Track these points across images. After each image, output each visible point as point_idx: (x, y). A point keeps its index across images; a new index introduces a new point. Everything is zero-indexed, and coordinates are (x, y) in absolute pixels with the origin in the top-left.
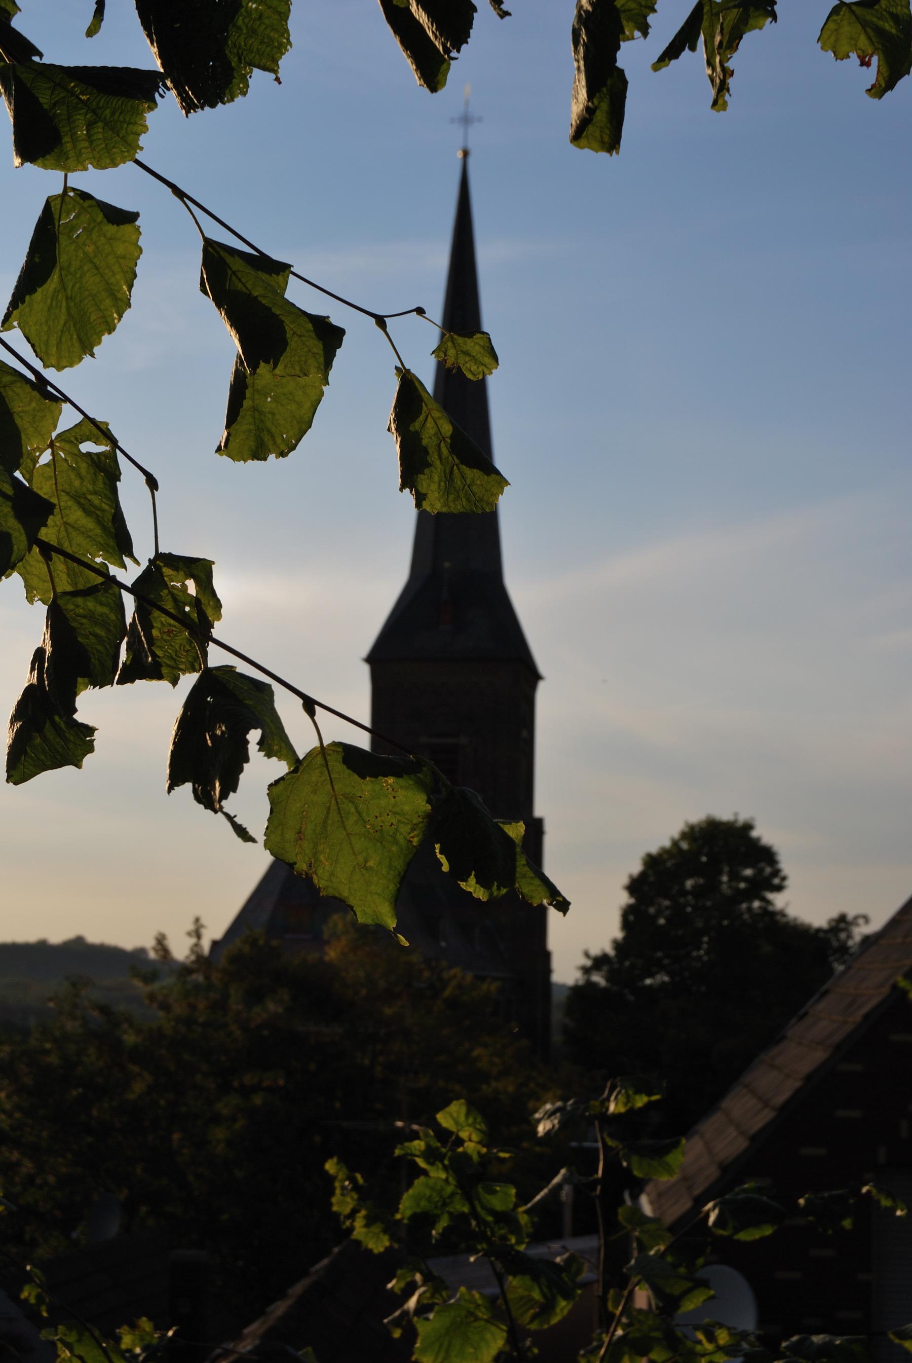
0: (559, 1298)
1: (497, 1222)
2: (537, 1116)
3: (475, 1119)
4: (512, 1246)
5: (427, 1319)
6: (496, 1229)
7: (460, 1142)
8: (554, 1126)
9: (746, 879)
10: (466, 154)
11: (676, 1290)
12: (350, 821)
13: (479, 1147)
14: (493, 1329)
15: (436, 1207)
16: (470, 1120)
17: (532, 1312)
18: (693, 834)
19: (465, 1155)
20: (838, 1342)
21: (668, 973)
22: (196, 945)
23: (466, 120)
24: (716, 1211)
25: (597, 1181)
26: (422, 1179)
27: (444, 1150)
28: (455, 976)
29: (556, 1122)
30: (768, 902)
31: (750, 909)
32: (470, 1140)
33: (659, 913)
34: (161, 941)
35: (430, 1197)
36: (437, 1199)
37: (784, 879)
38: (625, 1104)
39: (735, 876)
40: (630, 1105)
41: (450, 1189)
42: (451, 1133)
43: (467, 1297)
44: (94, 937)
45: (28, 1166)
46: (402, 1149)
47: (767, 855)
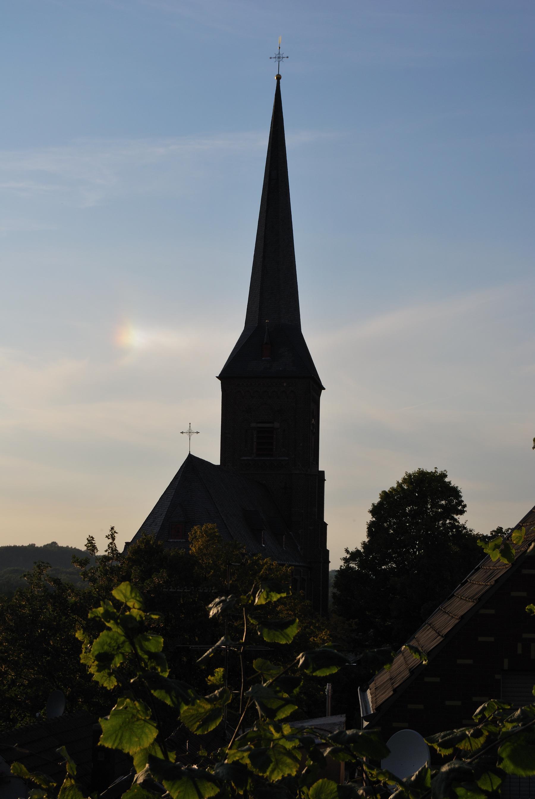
0: (183, 704)
1: (149, 659)
2: (210, 606)
3: (136, 594)
4: (159, 673)
5: (107, 719)
6: (149, 664)
8: (218, 611)
9: (442, 506)
10: (279, 78)
11: (274, 706)
13: (141, 612)
14: (150, 726)
15: (114, 650)
16: (133, 595)
17: (198, 723)
18: (410, 479)
19: (131, 617)
20: (360, 734)
22: (111, 543)
23: (279, 58)
24: (303, 658)
25: (242, 644)
26: (105, 632)
27: (118, 614)
28: (266, 563)
29: (219, 608)
30: (456, 520)
31: (444, 524)
32: (134, 608)
33: (390, 527)
34: (91, 542)
35: (110, 643)
36: (114, 645)
37: (465, 506)
38: (266, 599)
39: (435, 505)
40: (269, 600)
41: (122, 639)
42: (122, 603)
43: (131, 706)
44: (62, 543)
45: (12, 675)
46: (92, 613)
47: (455, 493)
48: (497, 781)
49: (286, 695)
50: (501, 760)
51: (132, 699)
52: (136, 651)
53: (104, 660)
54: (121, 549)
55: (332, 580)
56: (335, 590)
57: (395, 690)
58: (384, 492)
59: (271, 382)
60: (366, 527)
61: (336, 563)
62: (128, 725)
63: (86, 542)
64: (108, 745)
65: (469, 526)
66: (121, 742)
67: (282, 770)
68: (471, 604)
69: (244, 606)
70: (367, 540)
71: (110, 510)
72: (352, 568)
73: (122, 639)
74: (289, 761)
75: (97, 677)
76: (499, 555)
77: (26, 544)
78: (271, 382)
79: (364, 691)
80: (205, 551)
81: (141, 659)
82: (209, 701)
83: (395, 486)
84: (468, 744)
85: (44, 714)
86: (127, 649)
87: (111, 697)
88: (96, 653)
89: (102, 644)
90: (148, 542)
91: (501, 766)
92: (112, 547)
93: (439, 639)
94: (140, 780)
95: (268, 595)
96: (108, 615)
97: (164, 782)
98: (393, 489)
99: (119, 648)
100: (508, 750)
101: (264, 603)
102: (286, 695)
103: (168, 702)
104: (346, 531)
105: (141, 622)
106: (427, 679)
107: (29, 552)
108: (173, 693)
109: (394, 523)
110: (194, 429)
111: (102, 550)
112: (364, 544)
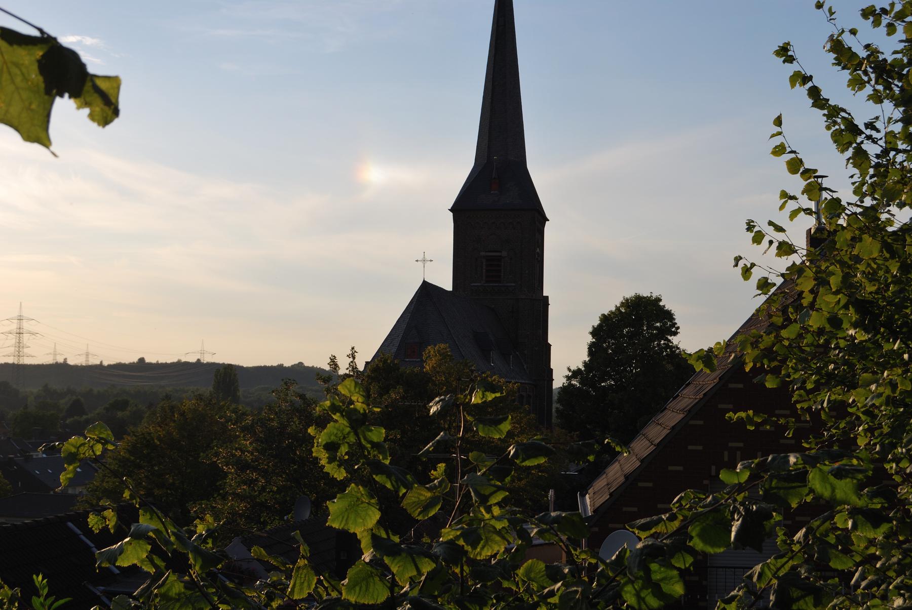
1: (372, 448)
7: (352, 402)
9: (657, 328)
11: (487, 493)
12: (18, 80)
13: (364, 406)
18: (627, 303)
19: (355, 410)
21: (614, 380)
30: (669, 341)
31: (659, 345)
34: (333, 363)
37: (678, 328)
44: (308, 363)
47: (669, 315)
48: (690, 560)
49: (499, 483)
50: (691, 538)
51: (357, 485)
52: (359, 439)
53: (331, 447)
54: (361, 367)
55: (555, 397)
56: (558, 406)
57: (611, 494)
58: (603, 315)
59: (499, 214)
60: (587, 347)
61: (559, 381)
62: (353, 508)
63: (329, 361)
64: (336, 525)
65: (682, 346)
66: (347, 523)
67: (491, 547)
68: (682, 416)
69: (461, 404)
70: (587, 359)
71: (348, 331)
72: (574, 385)
73: (348, 429)
74: (498, 538)
75: (328, 468)
76: (702, 366)
77: (275, 364)
78: (499, 214)
79: (583, 496)
80: (438, 369)
81: (363, 448)
82: (429, 489)
83: (614, 309)
84: (664, 528)
85: (292, 517)
86: (352, 439)
87: (342, 486)
88: (324, 443)
89: (330, 435)
90: (385, 361)
91: (691, 544)
92: (353, 367)
93: (652, 448)
94: (367, 560)
95: (483, 395)
96: (334, 408)
97: (385, 558)
98: (611, 312)
99: (344, 438)
100: (698, 529)
101: (480, 402)
102: (499, 483)
103: (389, 486)
104: (568, 350)
105: (365, 414)
106: (640, 484)
107: (278, 371)
108: (393, 478)
109: (613, 344)
110: (428, 258)
111: (343, 370)
112: (585, 362)
